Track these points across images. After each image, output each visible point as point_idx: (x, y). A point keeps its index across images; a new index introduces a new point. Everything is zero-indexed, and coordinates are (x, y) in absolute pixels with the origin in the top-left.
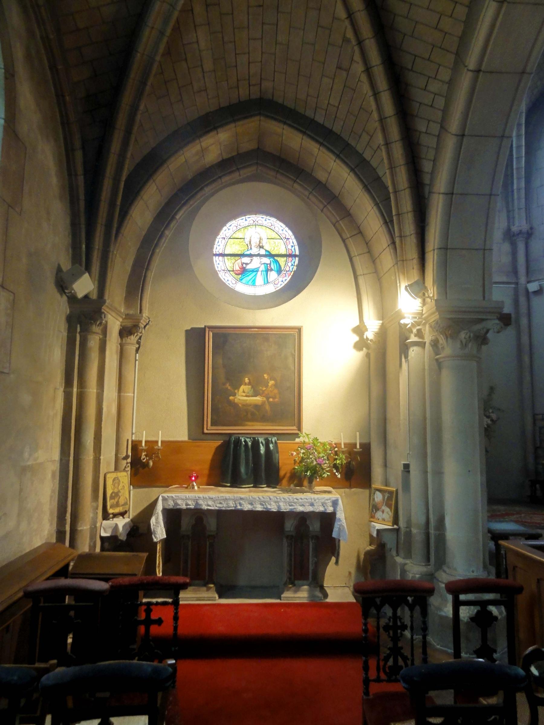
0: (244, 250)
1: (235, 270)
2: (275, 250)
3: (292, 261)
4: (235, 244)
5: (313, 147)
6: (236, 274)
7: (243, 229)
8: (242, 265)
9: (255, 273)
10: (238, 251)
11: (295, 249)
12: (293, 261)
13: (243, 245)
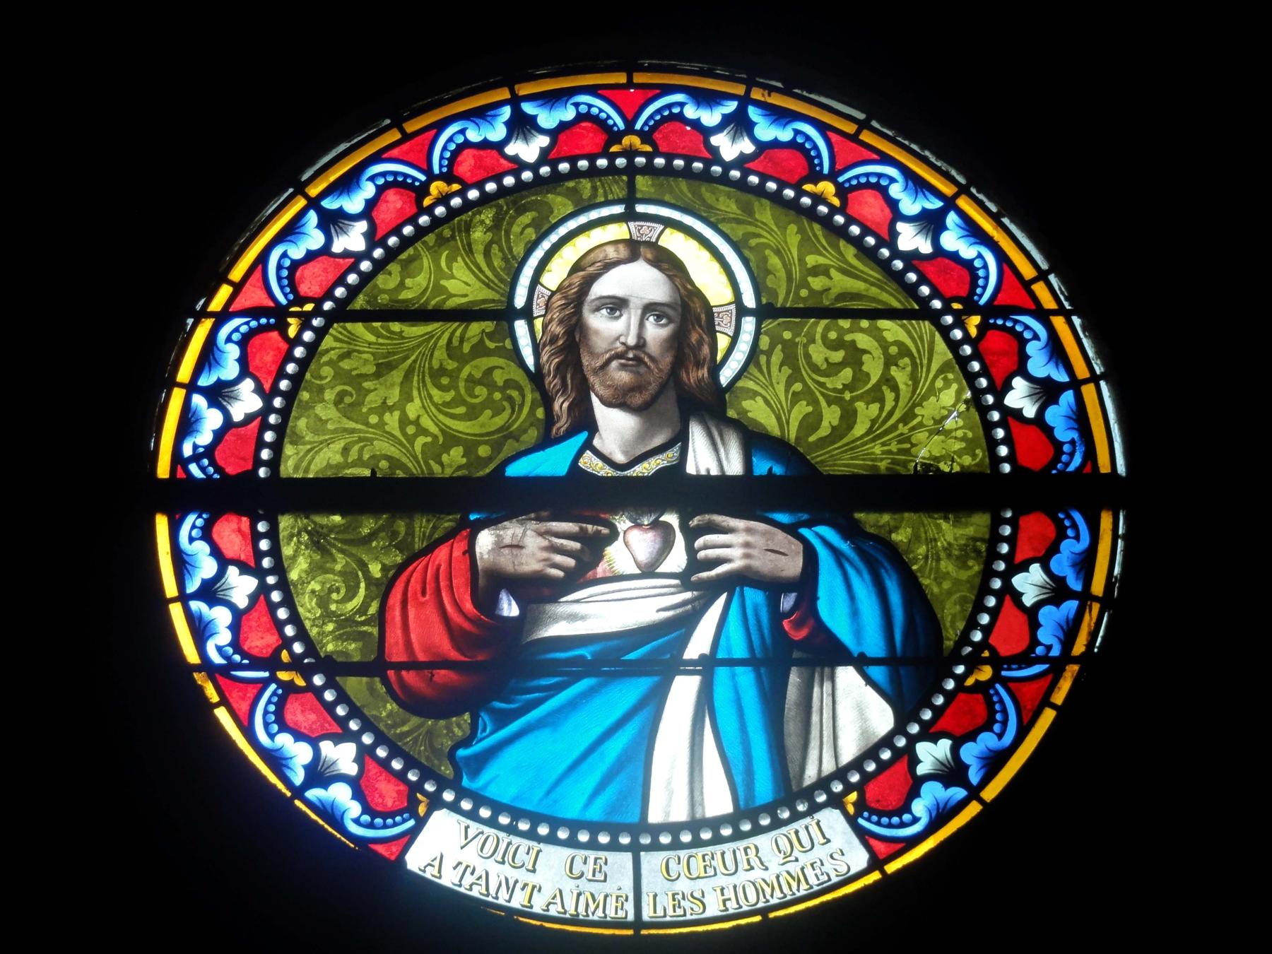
0: (506, 434)
1: (396, 653)
2: (860, 429)
3: (1054, 549)
4: (397, 376)
5: (751, 628)
6: (412, 703)
7: (487, 216)
8: (487, 603)
9: (627, 693)
10: (435, 451)
11: (1080, 418)
12: (1070, 547)
13: (486, 379)
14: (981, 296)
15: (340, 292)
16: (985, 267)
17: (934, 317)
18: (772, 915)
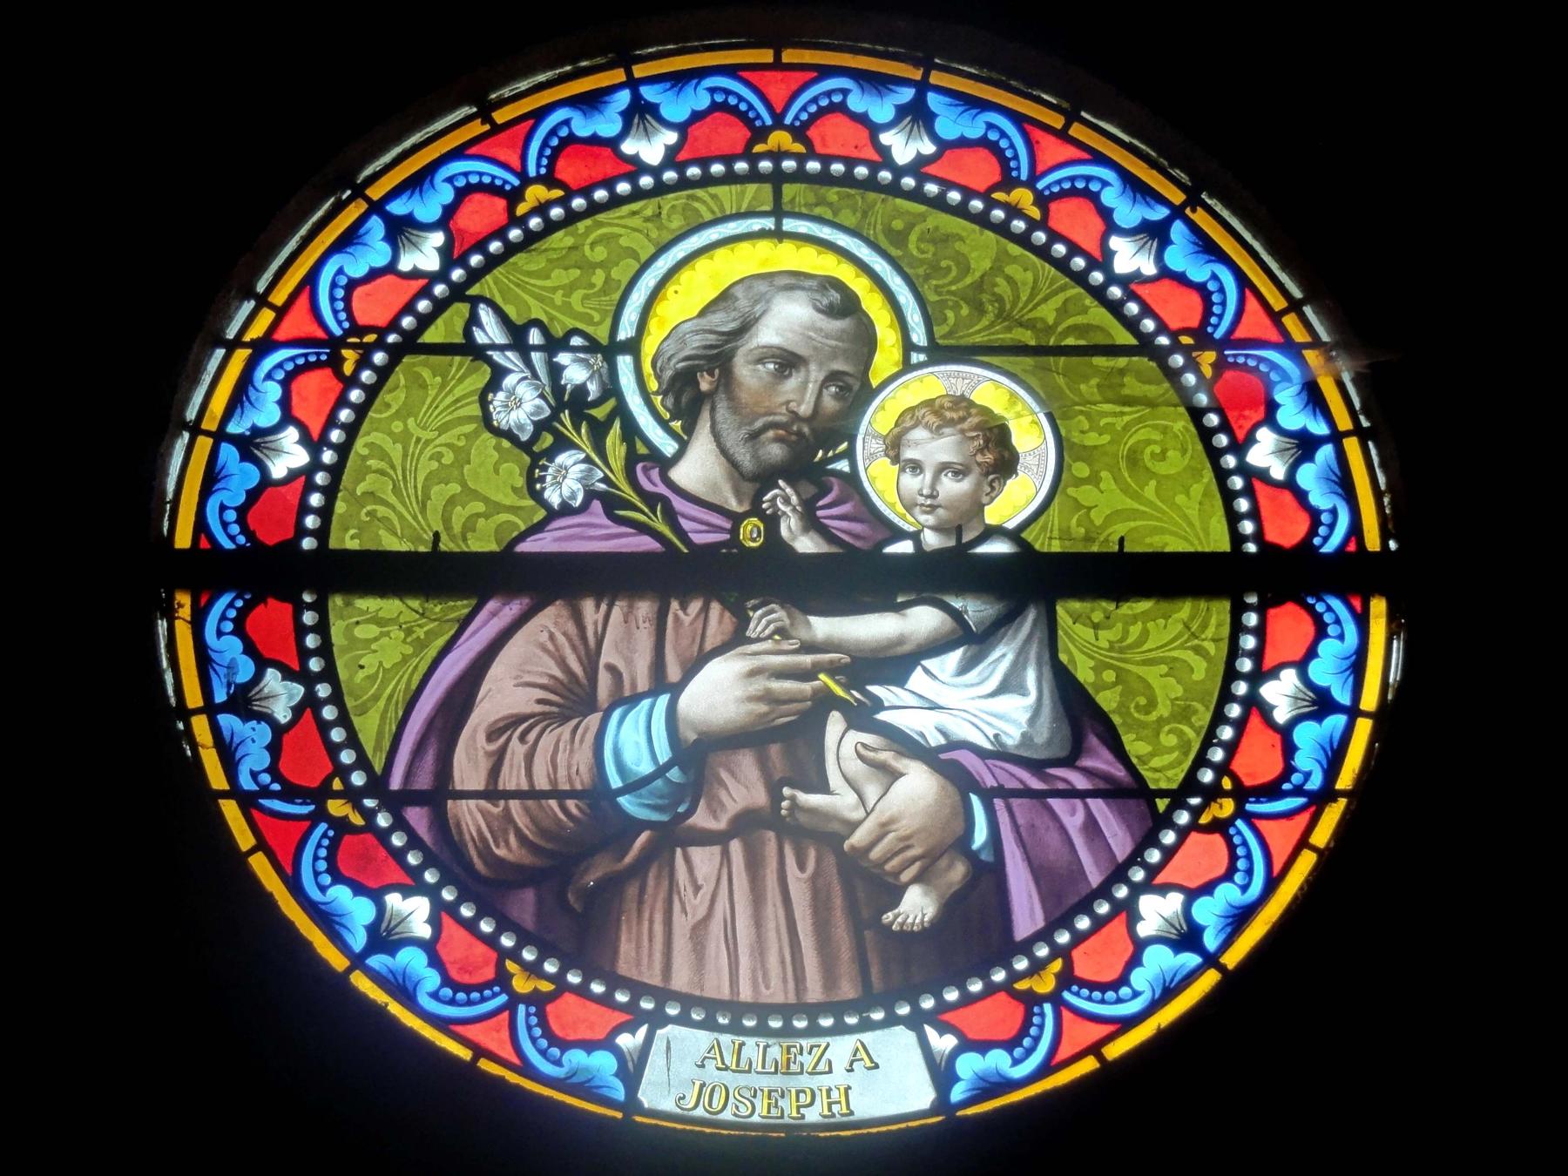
14: (1216, 327)
15: (407, 322)
16: (1222, 290)
17: (1160, 356)
18: (1383, 487)
